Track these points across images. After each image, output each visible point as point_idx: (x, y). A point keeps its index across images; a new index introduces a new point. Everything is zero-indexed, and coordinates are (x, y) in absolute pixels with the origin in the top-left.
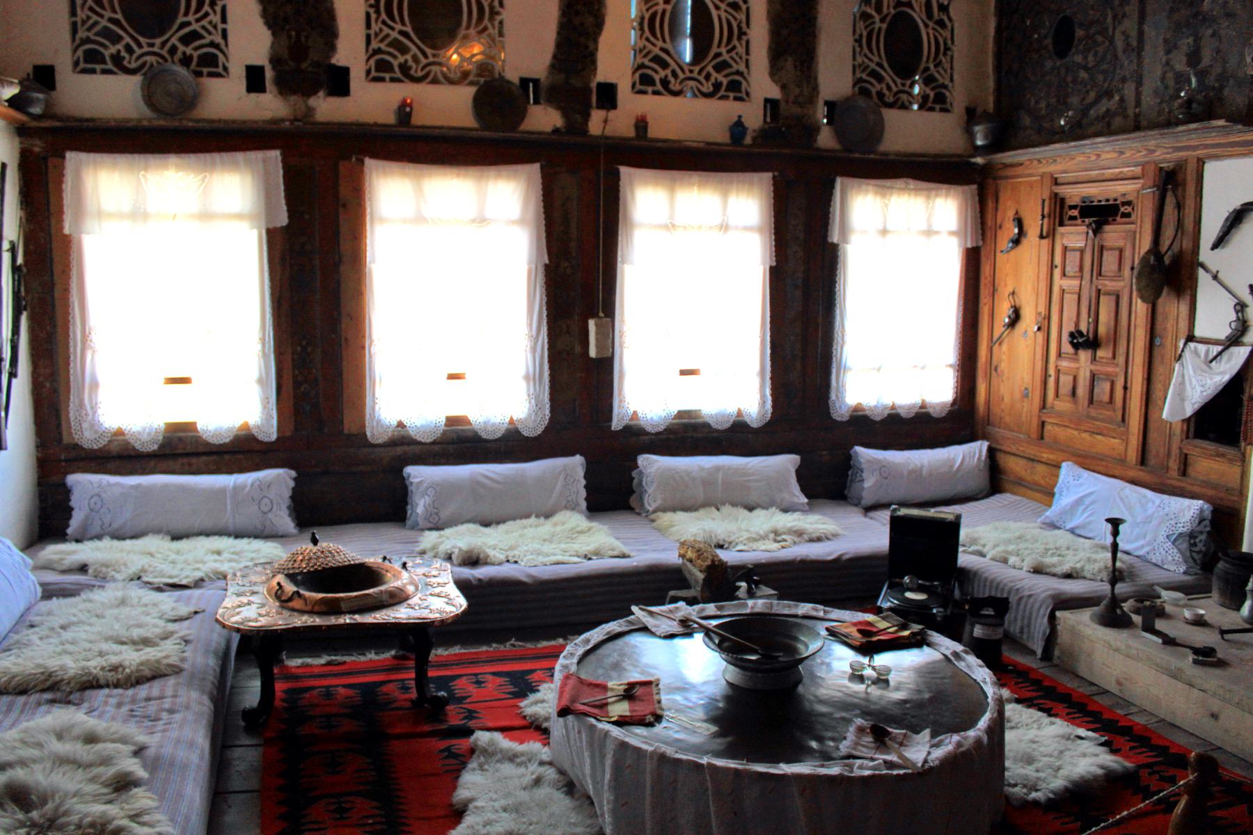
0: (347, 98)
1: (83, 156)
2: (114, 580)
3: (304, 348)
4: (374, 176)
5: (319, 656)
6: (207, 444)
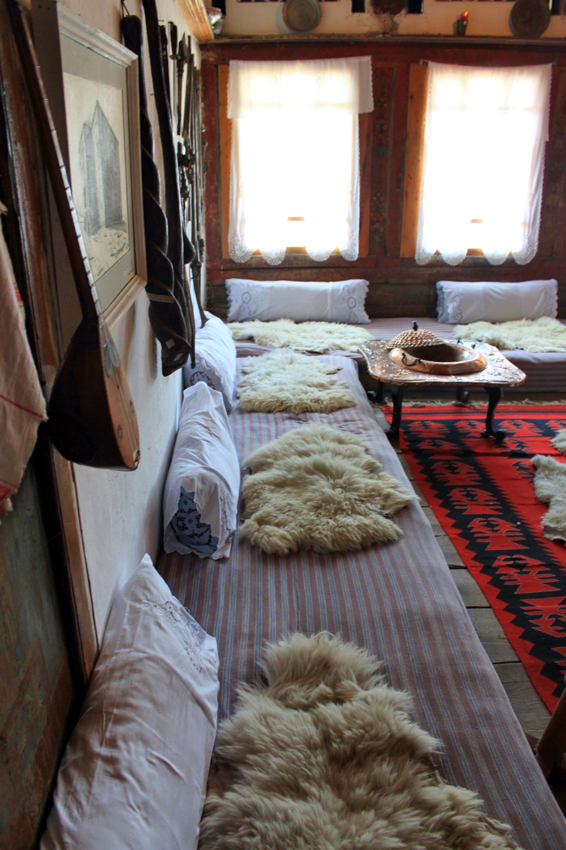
0: (420, 15)
1: (241, 63)
2: (274, 348)
3: (378, 199)
4: (434, 73)
5: (408, 402)
6: (313, 261)
